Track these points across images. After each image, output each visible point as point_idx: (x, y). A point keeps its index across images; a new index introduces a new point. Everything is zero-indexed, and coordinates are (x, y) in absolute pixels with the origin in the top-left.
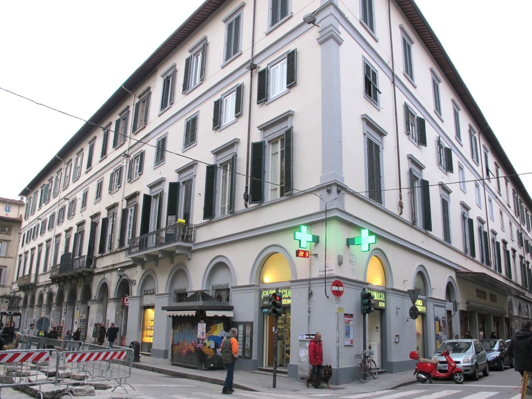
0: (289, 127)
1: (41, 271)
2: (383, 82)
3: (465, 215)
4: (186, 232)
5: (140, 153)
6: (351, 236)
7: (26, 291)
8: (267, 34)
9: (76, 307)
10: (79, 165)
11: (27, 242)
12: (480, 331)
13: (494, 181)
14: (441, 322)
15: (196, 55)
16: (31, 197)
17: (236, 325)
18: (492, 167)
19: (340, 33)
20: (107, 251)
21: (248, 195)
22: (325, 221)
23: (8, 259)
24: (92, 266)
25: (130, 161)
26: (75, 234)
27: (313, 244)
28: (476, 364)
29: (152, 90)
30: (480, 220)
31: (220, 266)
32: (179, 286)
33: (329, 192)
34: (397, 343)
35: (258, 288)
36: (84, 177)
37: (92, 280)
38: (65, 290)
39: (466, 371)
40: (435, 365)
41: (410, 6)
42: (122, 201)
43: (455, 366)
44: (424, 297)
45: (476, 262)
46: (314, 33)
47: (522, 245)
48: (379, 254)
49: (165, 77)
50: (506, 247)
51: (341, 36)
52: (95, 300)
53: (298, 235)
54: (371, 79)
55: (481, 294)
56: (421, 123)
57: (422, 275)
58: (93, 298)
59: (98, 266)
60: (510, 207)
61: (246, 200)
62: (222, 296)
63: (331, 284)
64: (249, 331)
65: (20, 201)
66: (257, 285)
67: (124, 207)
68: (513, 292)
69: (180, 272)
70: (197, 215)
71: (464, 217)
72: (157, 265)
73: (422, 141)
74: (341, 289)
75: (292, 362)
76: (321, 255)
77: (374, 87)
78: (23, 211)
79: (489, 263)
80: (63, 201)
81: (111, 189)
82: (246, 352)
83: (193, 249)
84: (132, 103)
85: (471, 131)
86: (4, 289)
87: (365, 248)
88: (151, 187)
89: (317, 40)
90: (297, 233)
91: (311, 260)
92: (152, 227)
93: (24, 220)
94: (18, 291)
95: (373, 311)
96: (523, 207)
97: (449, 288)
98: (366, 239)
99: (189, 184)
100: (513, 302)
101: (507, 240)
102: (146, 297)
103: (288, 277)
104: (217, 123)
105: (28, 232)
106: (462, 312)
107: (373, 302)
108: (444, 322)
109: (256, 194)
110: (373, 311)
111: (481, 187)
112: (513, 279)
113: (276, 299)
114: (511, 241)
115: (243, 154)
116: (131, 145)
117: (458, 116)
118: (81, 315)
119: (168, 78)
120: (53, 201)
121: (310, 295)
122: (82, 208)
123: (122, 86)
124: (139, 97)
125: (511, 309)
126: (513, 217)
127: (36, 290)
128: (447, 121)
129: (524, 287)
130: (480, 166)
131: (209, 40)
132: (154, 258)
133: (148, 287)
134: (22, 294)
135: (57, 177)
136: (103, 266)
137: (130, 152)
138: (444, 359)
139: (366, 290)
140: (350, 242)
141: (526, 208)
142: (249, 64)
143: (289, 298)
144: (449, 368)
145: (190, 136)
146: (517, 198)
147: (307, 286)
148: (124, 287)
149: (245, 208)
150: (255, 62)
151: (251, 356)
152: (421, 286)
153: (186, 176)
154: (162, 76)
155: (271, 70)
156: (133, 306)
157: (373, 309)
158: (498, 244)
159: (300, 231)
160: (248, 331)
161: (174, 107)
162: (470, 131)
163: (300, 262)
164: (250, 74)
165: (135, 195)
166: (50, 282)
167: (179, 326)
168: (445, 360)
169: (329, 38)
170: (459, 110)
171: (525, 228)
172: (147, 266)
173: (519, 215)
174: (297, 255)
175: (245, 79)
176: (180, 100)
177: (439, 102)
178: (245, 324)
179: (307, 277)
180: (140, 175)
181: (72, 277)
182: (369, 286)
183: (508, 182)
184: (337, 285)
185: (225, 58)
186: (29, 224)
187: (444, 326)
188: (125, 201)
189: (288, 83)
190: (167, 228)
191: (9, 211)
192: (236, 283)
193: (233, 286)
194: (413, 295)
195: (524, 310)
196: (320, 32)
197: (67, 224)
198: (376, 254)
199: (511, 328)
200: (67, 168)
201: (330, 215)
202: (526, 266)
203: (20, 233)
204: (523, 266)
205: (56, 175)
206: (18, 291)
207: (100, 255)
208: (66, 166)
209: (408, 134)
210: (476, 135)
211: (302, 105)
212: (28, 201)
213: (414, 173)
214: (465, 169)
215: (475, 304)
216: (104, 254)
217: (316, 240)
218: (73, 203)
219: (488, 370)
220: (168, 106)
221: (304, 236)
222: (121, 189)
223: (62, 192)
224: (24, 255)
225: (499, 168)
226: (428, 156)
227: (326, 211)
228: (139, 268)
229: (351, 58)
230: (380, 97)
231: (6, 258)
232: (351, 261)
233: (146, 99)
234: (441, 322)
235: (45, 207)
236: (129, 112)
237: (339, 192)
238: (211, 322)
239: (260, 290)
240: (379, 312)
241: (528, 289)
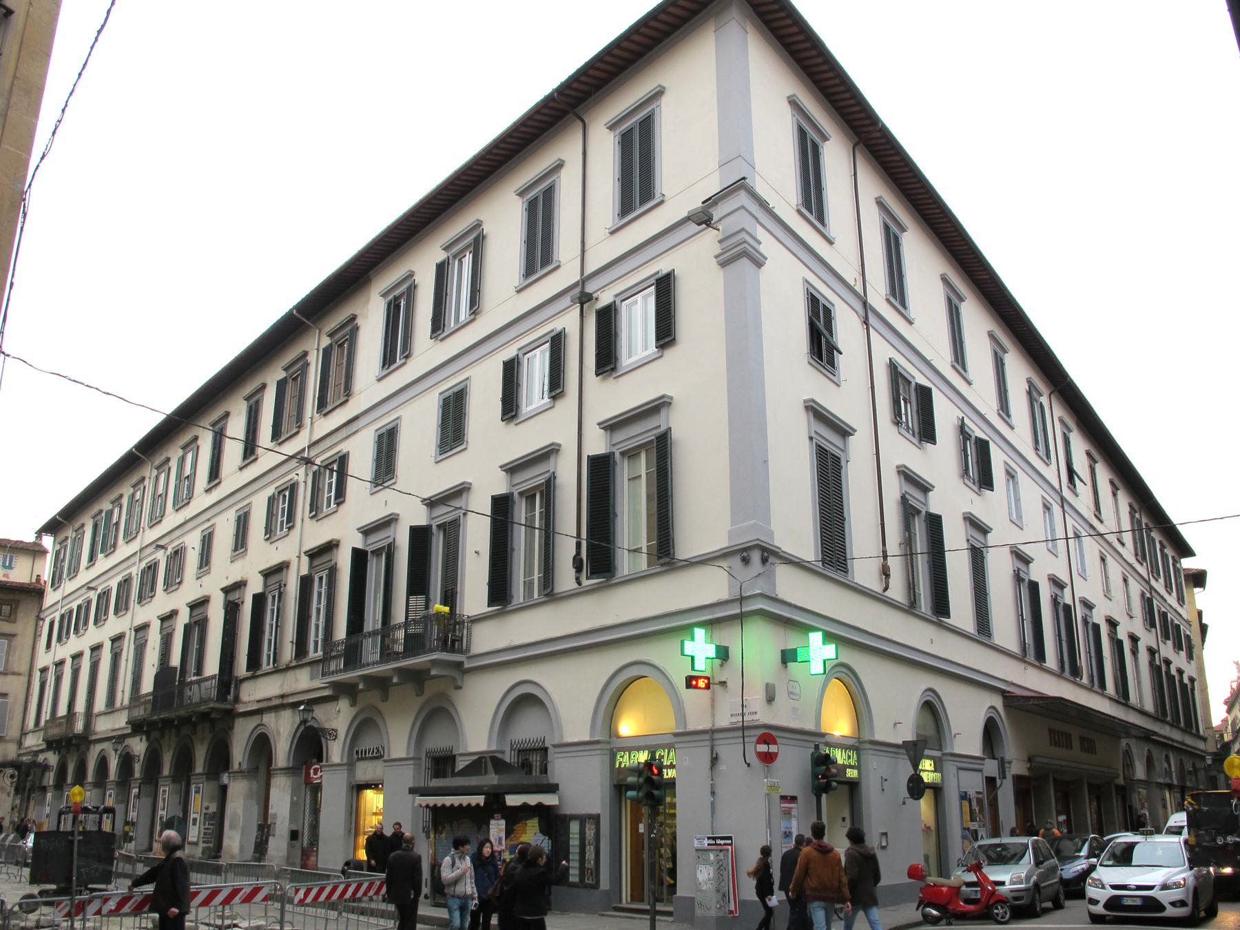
0: (663, 429)
1: (100, 704)
2: (846, 328)
3: (1022, 575)
4: (452, 632)
6: (790, 646)
7: (63, 751)
8: (612, 233)
9: (193, 787)
10: (188, 471)
11: (59, 639)
12: (1059, 813)
13: (1084, 490)
14: (974, 803)
15: (459, 256)
16: (67, 538)
17: (566, 820)
18: (1081, 464)
19: (760, 243)
20: (265, 667)
21: (581, 560)
22: (741, 618)
23: (10, 678)
24: (231, 697)
25: (314, 473)
26: (186, 626)
27: (718, 662)
28: (1036, 885)
29: (359, 321)
30: (1056, 582)
31: (525, 702)
32: (438, 741)
33: (746, 561)
34: (883, 848)
35: (608, 747)
36: (201, 501)
37: (231, 728)
38: (165, 749)
39: (1016, 899)
40: (956, 891)
41: (897, 158)
42: (299, 557)
43: (993, 893)
44: (937, 754)
45: (1049, 671)
46: (707, 243)
47: (1153, 625)
48: (842, 672)
49: (391, 297)
50: (1116, 633)
51: (762, 249)
52: (241, 772)
53: (689, 648)
54: (821, 325)
55: (1059, 739)
56: (924, 396)
57: (931, 708)
58: (236, 767)
59: (244, 696)
60: (1123, 544)
61: (579, 569)
62: (531, 764)
63: (754, 739)
64: (592, 832)
65: (35, 543)
66: (609, 743)
67: (305, 571)
68: (1133, 732)
69: (439, 712)
70: (474, 594)
71: (1018, 579)
72: (385, 698)
73: (927, 433)
74: (773, 748)
75: (681, 891)
76: (734, 685)
77: (827, 342)
78: (46, 570)
79: (1076, 671)
80: (151, 549)
81: (269, 530)
82: (588, 874)
83: (466, 666)
84: (314, 346)
85: (1032, 393)
87: (817, 668)
88: (367, 531)
89: (716, 257)
90: (686, 643)
91: (713, 693)
92: (373, 619)
93: (49, 589)
94: (42, 751)
95: (835, 789)
96: (1153, 540)
97: (991, 732)
98: (818, 652)
99: (452, 530)
100: (1134, 750)
101: (1116, 617)
103: (669, 724)
104: (510, 407)
105: (62, 617)
106: (1018, 779)
107: (834, 771)
108: (979, 801)
109: (599, 561)
110: (835, 789)
111: (1056, 509)
112: (1133, 698)
113: (653, 773)
114: (1127, 618)
115: (568, 476)
116: (316, 437)
117: (1003, 364)
118: (205, 804)
119: (397, 299)
120: (124, 550)
121: (714, 760)
122: (201, 567)
123: (291, 311)
124: (331, 335)
125: (1129, 765)
126: (1130, 565)
127: (88, 749)
128: (982, 383)
129: (1159, 717)
130: (1054, 466)
131: (487, 228)
132: (380, 684)
133: (368, 743)
134: (52, 758)
135: (133, 495)
137: (313, 453)
138: (972, 877)
139: (821, 746)
140: (787, 657)
141: (1161, 542)
142: (577, 290)
143: (672, 766)
144: (982, 895)
145: (450, 429)
146: (1139, 522)
147: (708, 743)
148: (311, 745)
149: (576, 586)
151: (598, 882)
152: (930, 731)
153: (444, 514)
154: (384, 295)
155: (624, 308)
156: (333, 785)
157: (834, 784)
158: (1096, 628)
159: (692, 639)
160: (590, 833)
161: (411, 363)
162: (1029, 393)
163: (695, 700)
164: (578, 310)
165: (331, 547)
166: (129, 731)
167: (447, 827)
168: (975, 879)
169: (739, 255)
170: (1005, 352)
171: (1159, 586)
172: (363, 700)
173: (1144, 558)
174: (689, 686)
175: (568, 321)
176: (427, 351)
177: (961, 343)
178: (583, 819)
179: (706, 725)
180: (338, 504)
181: (186, 721)
182: (827, 739)
183: (1118, 489)
184: (765, 742)
185: (523, 272)
186: (64, 598)
187: (981, 810)
188: (305, 560)
189: (658, 339)
190: (406, 624)
191: (10, 567)
192: (562, 736)
193: (556, 742)
194: (914, 751)
195: (1160, 765)
196: (720, 242)
197: (162, 602)
198: (837, 675)
199: (1130, 807)
200: (157, 478)
201: (748, 608)
202: (1164, 669)
203: (39, 619)
204: (1155, 670)
205: (132, 490)
206: (42, 751)
207: (249, 674)
208: (155, 472)
209: (897, 423)
210: (1044, 400)
211: (686, 382)
212: (58, 547)
213: (912, 502)
214: (1021, 476)
215: (1046, 761)
216: (259, 673)
217: (723, 654)
218: (178, 555)
219: (1062, 896)
220: (399, 362)
221: (700, 648)
222: (295, 533)
223: (148, 531)
224: (52, 669)
225: (1096, 462)
226: (940, 463)
227: (742, 600)
228: (343, 705)
229: (782, 285)
230: (840, 360)
231: (6, 674)
232: (790, 693)
233: (347, 337)
234: (974, 803)
235: (103, 563)
236: (308, 364)
237: (764, 561)
238: (515, 817)
239: (611, 750)
240: (846, 788)
241: (1169, 718)
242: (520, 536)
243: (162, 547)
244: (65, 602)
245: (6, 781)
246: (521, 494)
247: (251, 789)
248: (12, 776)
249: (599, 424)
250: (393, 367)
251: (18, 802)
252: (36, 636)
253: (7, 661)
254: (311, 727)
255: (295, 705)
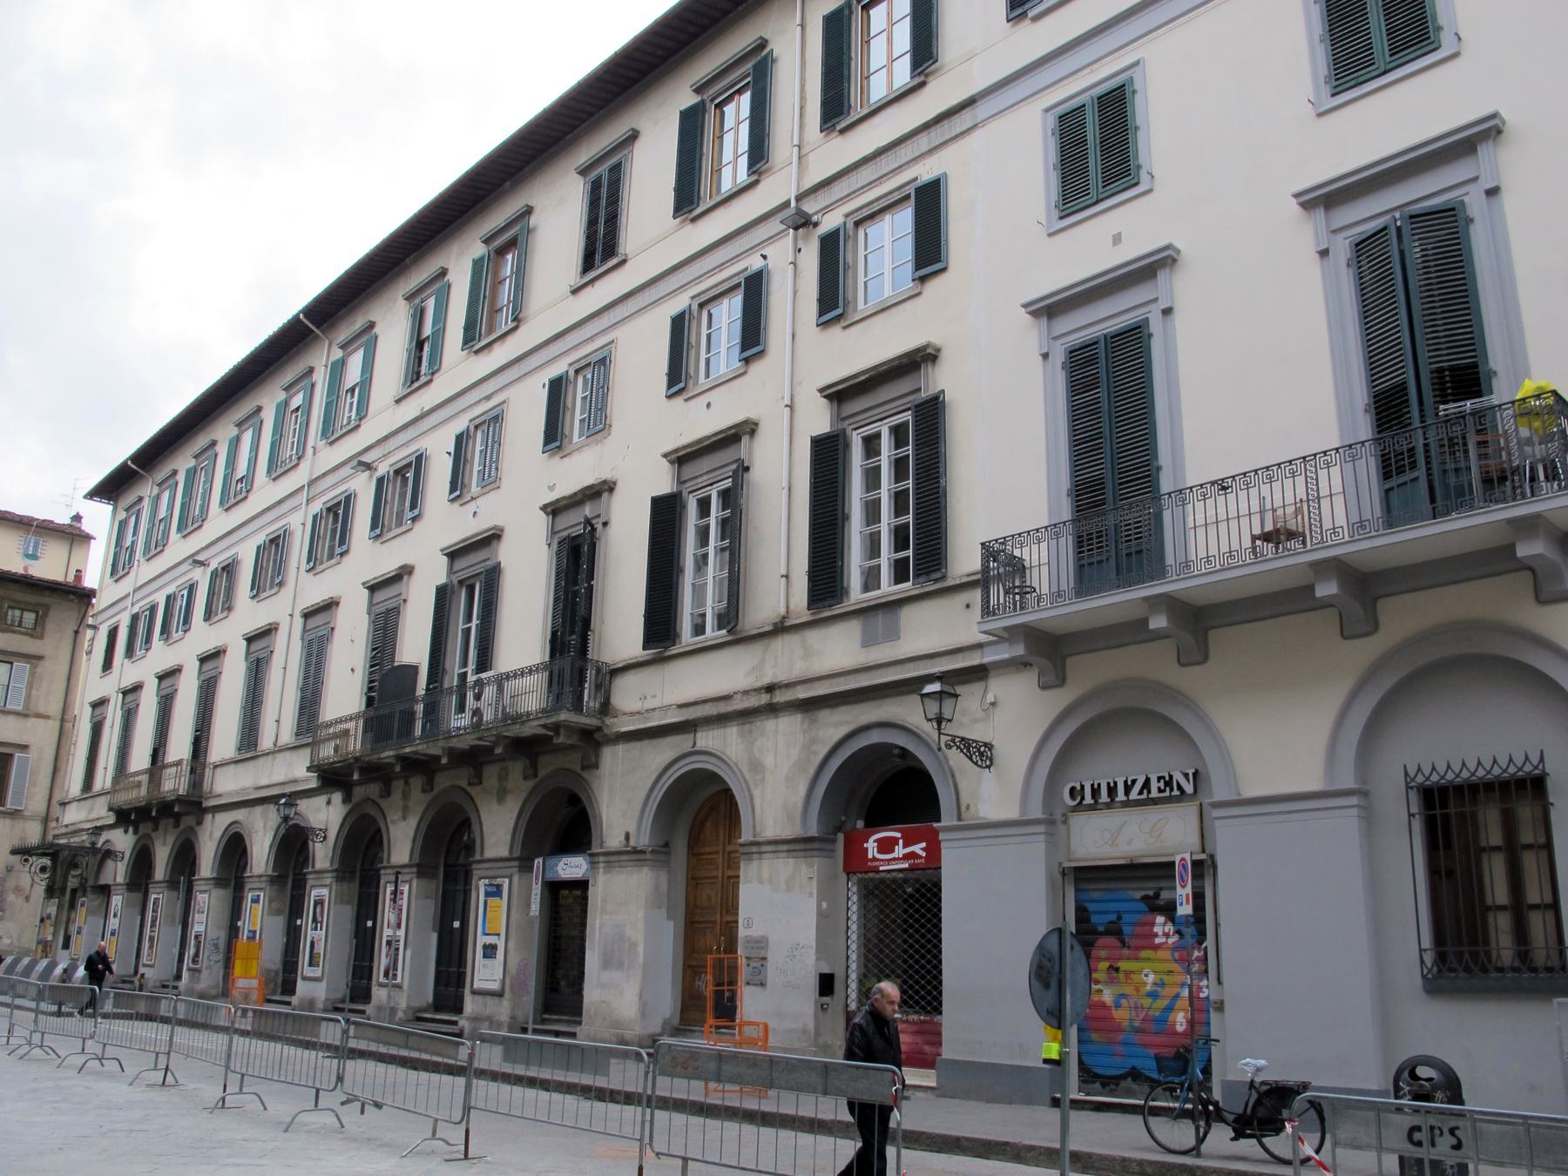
1: (224, 741)
5: (741, 279)
11: (130, 652)
23: (32, 720)
38: (393, 816)
58: (614, 841)
72: (156, 829)
84: (459, 261)
86: (19, 824)
102: (1079, 821)
105: (135, 618)
123: (297, 316)
134: (123, 841)
136: (682, 701)
150: (809, 207)
161: (438, 380)
166: (313, 784)
176: (458, 368)
191: (34, 557)
200: (158, 497)
208: (156, 490)
212: (122, 515)
216: (674, 650)
220: (423, 379)
231: (26, 716)
233: (512, 242)
242: (458, 624)
243: (202, 564)
244: (138, 595)
245: (31, 880)
246: (461, 582)
247: (657, 887)
248: (43, 869)
249: (1025, 306)
250: (416, 385)
251: (52, 910)
252: (403, 496)
253: (29, 696)
254: (296, 826)
255: (273, 800)
